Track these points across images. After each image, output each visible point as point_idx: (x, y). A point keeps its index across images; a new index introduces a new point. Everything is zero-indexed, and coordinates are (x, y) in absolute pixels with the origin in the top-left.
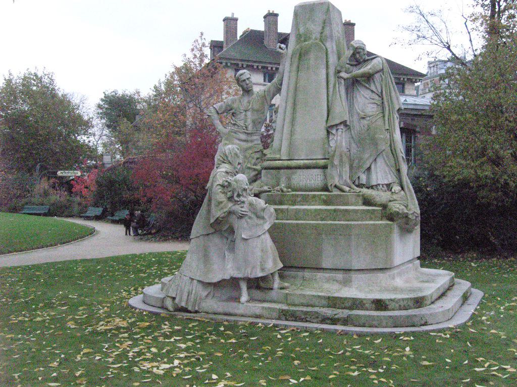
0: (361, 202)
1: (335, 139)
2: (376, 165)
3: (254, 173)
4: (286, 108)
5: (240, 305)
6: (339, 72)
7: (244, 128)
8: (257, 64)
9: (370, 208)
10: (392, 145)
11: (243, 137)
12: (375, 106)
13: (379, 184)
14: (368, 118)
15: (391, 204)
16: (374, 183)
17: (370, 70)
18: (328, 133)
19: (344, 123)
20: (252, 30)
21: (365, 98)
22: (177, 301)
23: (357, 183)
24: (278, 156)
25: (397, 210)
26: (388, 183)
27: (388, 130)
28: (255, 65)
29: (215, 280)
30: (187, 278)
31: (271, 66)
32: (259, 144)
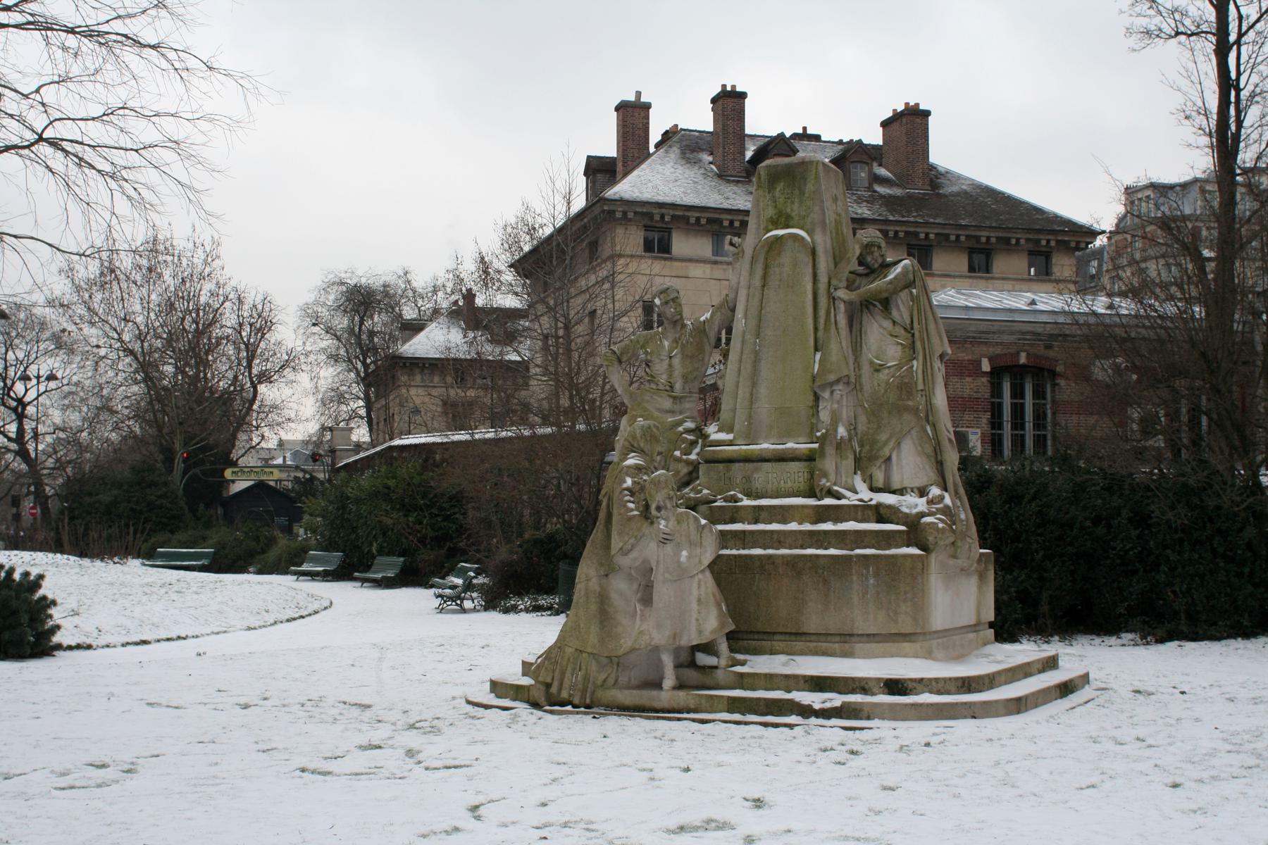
3: (685, 470)
4: (742, 353)
22: (554, 689)
31: (730, 217)
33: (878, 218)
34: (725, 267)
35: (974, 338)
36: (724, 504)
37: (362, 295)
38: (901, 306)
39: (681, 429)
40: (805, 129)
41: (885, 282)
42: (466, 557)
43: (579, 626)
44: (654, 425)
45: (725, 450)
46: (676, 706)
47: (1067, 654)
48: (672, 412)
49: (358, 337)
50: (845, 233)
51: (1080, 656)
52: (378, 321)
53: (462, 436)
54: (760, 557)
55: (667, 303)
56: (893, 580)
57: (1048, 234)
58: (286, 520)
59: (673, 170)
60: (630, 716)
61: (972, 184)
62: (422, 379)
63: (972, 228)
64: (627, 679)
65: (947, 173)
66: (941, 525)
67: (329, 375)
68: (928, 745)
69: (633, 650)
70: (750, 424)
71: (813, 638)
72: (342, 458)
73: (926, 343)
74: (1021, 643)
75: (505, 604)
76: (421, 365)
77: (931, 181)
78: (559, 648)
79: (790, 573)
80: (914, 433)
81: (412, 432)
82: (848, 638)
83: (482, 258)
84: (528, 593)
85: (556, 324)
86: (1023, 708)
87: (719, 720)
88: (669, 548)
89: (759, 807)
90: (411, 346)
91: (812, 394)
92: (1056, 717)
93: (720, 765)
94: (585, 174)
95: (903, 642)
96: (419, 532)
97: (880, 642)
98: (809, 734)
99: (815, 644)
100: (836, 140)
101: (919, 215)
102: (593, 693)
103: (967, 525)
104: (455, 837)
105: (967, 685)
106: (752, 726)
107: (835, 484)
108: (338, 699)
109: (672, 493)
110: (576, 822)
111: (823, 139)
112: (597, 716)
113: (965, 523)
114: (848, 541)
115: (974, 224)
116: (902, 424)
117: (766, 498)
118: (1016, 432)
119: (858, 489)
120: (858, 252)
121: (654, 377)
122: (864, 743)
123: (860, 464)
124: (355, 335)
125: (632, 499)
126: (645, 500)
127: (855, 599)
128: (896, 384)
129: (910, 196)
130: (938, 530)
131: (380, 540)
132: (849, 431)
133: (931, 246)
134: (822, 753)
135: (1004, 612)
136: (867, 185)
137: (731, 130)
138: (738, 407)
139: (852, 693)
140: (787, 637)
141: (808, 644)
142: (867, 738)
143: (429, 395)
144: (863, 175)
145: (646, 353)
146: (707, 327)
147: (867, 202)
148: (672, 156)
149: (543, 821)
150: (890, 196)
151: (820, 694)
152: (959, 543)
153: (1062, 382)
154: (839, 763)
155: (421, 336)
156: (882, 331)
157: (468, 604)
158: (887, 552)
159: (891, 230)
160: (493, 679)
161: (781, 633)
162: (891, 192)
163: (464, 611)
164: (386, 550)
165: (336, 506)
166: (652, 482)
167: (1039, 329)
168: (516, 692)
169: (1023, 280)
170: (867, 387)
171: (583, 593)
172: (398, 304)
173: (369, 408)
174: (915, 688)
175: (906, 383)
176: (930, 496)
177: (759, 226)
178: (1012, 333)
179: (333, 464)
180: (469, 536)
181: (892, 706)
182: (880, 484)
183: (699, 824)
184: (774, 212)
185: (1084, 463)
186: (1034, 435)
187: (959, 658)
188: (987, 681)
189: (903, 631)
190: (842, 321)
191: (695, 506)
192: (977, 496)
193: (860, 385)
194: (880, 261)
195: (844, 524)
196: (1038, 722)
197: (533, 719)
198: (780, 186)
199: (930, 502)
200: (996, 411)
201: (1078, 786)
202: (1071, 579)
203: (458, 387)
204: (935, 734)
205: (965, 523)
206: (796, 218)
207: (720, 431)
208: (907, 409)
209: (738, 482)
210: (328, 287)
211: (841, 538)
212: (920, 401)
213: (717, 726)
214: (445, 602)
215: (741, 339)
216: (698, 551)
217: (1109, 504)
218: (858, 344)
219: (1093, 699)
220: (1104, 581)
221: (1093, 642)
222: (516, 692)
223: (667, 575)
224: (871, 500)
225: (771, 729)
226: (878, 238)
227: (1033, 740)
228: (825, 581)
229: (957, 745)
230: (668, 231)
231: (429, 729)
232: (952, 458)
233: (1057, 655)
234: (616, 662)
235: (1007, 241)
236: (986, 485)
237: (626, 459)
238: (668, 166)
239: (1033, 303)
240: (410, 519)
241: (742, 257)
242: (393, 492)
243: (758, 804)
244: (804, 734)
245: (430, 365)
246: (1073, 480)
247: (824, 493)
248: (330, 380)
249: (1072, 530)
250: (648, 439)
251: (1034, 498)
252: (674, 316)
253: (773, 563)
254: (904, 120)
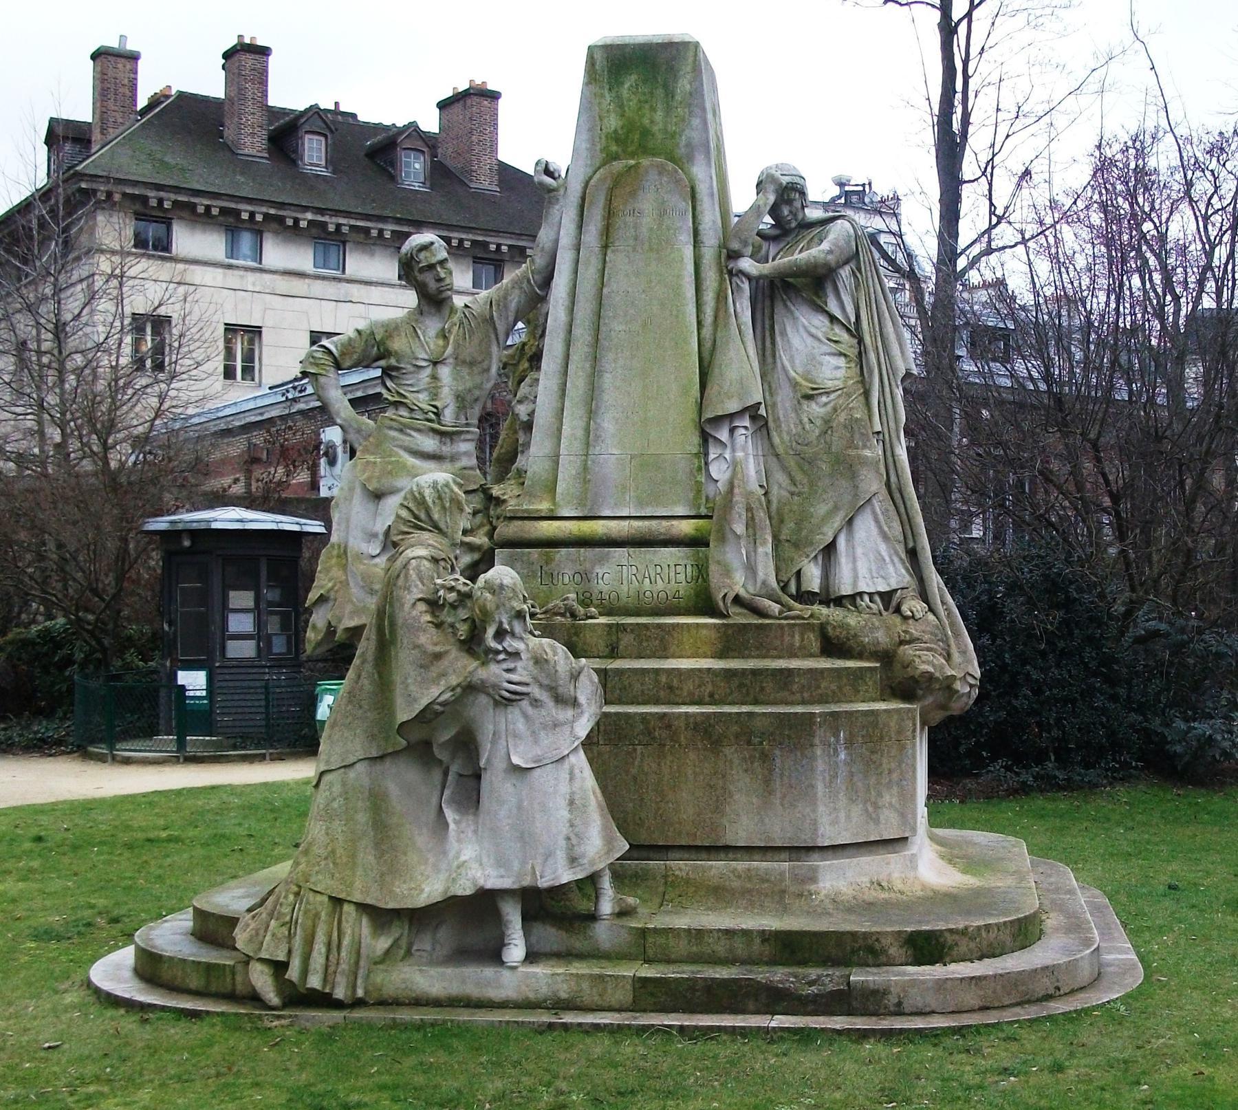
0: (814, 643)
1: (727, 456)
5: (506, 973)
6: (734, 255)
7: (432, 416)
9: (851, 664)
10: (893, 479)
11: (429, 443)
12: (842, 361)
13: (861, 594)
14: (824, 399)
15: (908, 651)
16: (846, 590)
17: (830, 257)
18: (705, 438)
19: (752, 411)
20: (182, 96)
21: (812, 336)
22: (293, 973)
23: (793, 588)
24: (544, 506)
25: (931, 669)
26: (888, 589)
27: (878, 433)
28: (201, 203)
29: (422, 900)
30: (319, 898)
31: (250, 208)
32: (471, 468)
34: (242, 273)
46: (531, 996)
56: (872, 752)
94: (46, 143)
114: (795, 687)
127: (820, 787)
133: (502, 261)
144: (417, 166)
174: (956, 944)
184: (620, 123)
198: (630, 81)
206: (660, 136)
209: (566, 580)
228: (765, 757)
253: (669, 727)
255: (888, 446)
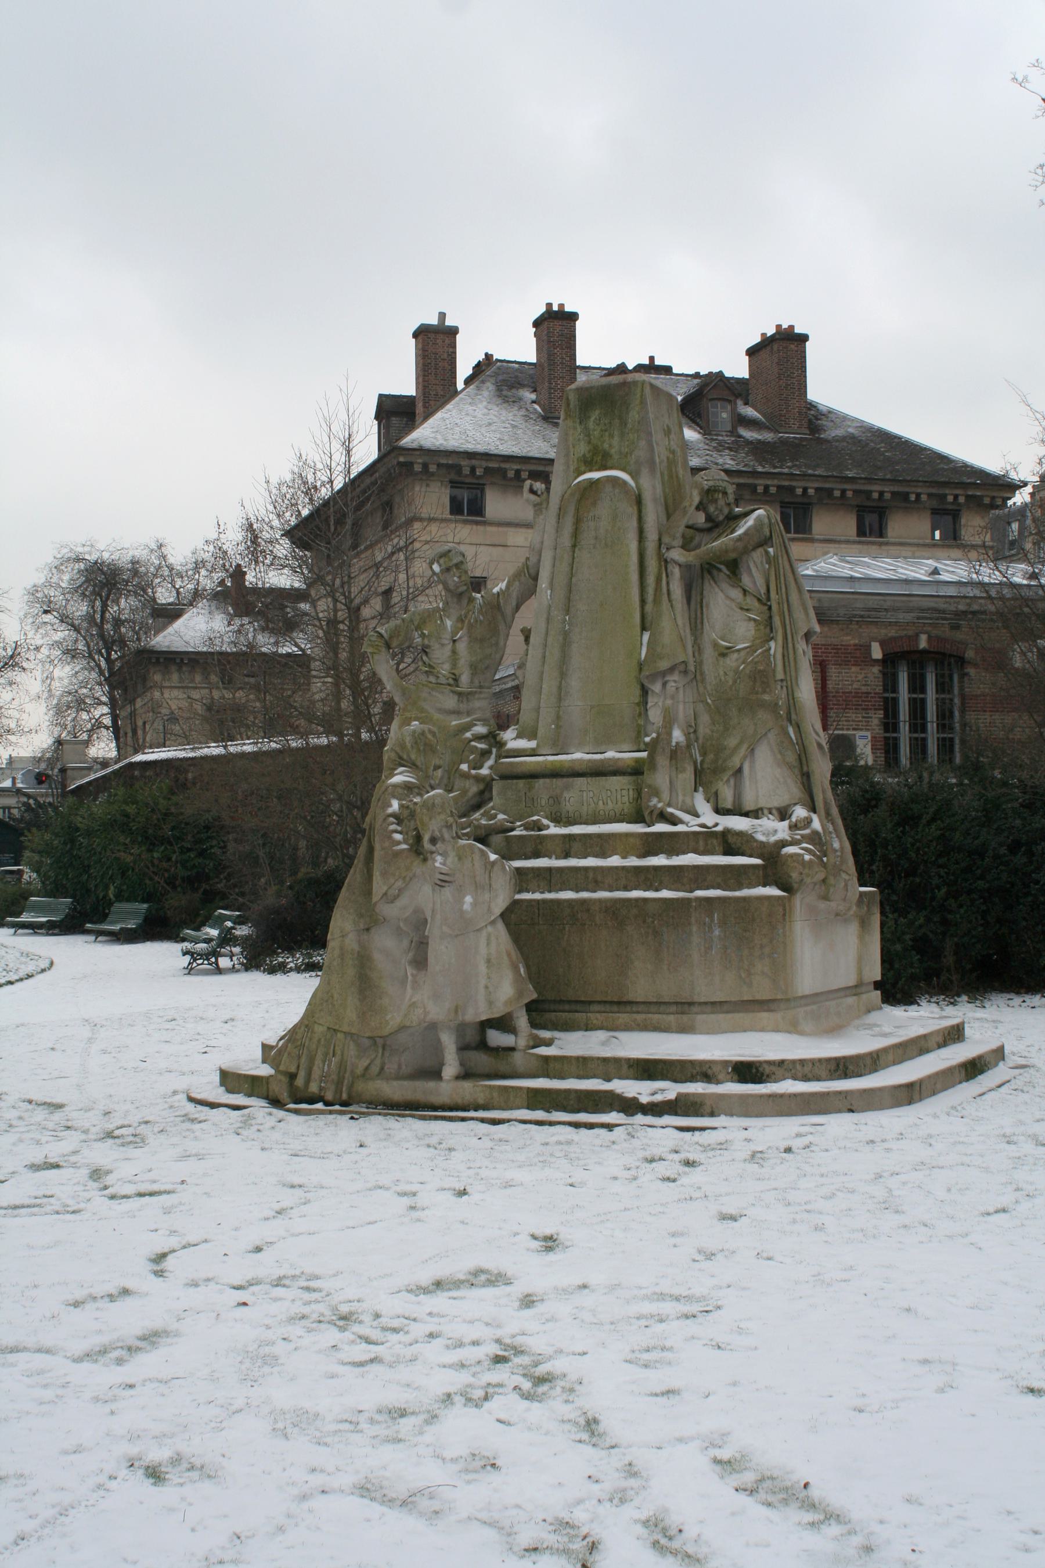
2: (753, 762)
3: (474, 789)
4: (547, 634)
8: (516, 467)
22: (300, 1082)
33: (744, 469)
35: (862, 616)
36: (524, 833)
37: (104, 573)
38: (754, 570)
39: (468, 735)
40: (652, 359)
41: (730, 539)
42: (226, 901)
43: (332, 997)
44: (430, 731)
45: (525, 762)
46: (460, 1101)
47: (978, 1019)
48: (457, 713)
49: (101, 627)
50: (681, 476)
51: (994, 1021)
52: (125, 606)
53: (215, 750)
54: (570, 902)
55: (448, 570)
57: (956, 488)
58: (12, 858)
59: (486, 411)
60: (399, 1115)
61: (861, 427)
62: (181, 678)
63: (863, 481)
64: (396, 1066)
65: (830, 412)
66: (807, 857)
67: (64, 674)
68: (788, 1150)
69: (402, 1028)
70: (558, 727)
71: (641, 1008)
72: (74, 779)
73: (787, 617)
74: (919, 1005)
75: (271, 962)
76: (178, 661)
77: (810, 421)
78: (307, 1026)
79: (610, 924)
80: (771, 736)
81: (168, 743)
82: (686, 1007)
83: (251, 525)
84: (300, 947)
85: (335, 606)
86: (916, 1096)
87: (516, 1120)
88: (447, 892)
89: (549, 1249)
90: (165, 637)
91: (639, 687)
92: (959, 1108)
93: (508, 1185)
94: (377, 417)
95: (759, 1011)
96: (166, 870)
97: (728, 1012)
98: (633, 1137)
99: (643, 1016)
100: (691, 372)
101: (796, 465)
102: (351, 1086)
103: (841, 857)
104: (129, 1301)
105: (842, 1067)
106: (558, 1128)
107: (669, 805)
108: (24, 1097)
109: (451, 820)
110: (294, 1276)
111: (675, 371)
112: (356, 1116)
113: (839, 854)
115: (863, 476)
116: (756, 724)
117: (581, 824)
118: (916, 735)
119: (700, 810)
120: (697, 500)
121: (434, 668)
122: (706, 1148)
123: (702, 778)
124: (96, 624)
125: (399, 828)
126: (416, 829)
128: (748, 672)
129: (783, 442)
130: (803, 863)
131: (118, 882)
132: (687, 735)
133: (810, 504)
134: (647, 1165)
135: (897, 966)
136: (729, 428)
137: (558, 360)
138: (542, 704)
139: (691, 1082)
140: (608, 1007)
141: (635, 1016)
142: (709, 1142)
143: (189, 697)
145: (423, 636)
146: (501, 601)
147: (730, 449)
148: (486, 393)
149: (249, 1277)
150: (759, 442)
151: (649, 1082)
152: (831, 880)
153: (971, 671)
154: (668, 1179)
155: (179, 624)
156: (728, 602)
157: (224, 962)
158: (737, 894)
159: (760, 485)
160: (223, 1067)
161: (600, 1002)
162: (760, 437)
163: (219, 971)
164: (126, 895)
165: (62, 839)
166: (425, 804)
167: (942, 606)
168: (252, 1085)
169: (925, 545)
170: (711, 678)
171: (337, 952)
172: (150, 585)
173: (115, 718)
174: (774, 1074)
175: (760, 671)
176: (794, 819)
177: (568, 467)
178: (910, 610)
179: (64, 786)
180: (229, 875)
181: (743, 1098)
182: (728, 804)
183: (462, 1277)
184: (587, 448)
185: (1000, 773)
186: (938, 739)
187: (834, 1030)
188: (868, 1061)
189: (758, 997)
190: (677, 589)
191: (487, 836)
192: (862, 817)
193: (702, 674)
194: (726, 511)
195: (682, 857)
196: (935, 1116)
197: (271, 1121)
198: (595, 414)
199: (793, 827)
200: (890, 708)
201: (982, 1209)
202: (982, 922)
203: (225, 688)
204: (799, 1135)
205: (839, 854)
206: (616, 457)
207: (519, 736)
208: (762, 705)
209: (543, 803)
210: (62, 564)
211: (676, 876)
212: (780, 694)
213: (512, 1128)
214: (195, 960)
215: (545, 616)
216: (487, 896)
217: (1030, 824)
218: (699, 621)
219: (1009, 1081)
220: (1024, 923)
221: (1011, 1003)
222: (252, 1085)
223: (445, 929)
224: (716, 825)
225: (583, 1132)
226: (723, 480)
227: (928, 1140)
228: (656, 933)
229: (827, 1150)
230: (481, 488)
231: (131, 1138)
232: (822, 768)
233: (963, 1023)
234: (381, 1044)
235: (905, 497)
236: (873, 803)
237: (393, 775)
238: (480, 406)
239: (936, 572)
240: (156, 855)
241: (547, 508)
242: (134, 820)
243: (550, 1244)
244: (627, 1137)
245: (190, 660)
246: (984, 795)
247: (654, 816)
248: (66, 681)
249: (983, 859)
250: (422, 748)
251: (933, 820)
252: (458, 587)
253: (588, 910)
254: (775, 347)
255: (790, 690)
